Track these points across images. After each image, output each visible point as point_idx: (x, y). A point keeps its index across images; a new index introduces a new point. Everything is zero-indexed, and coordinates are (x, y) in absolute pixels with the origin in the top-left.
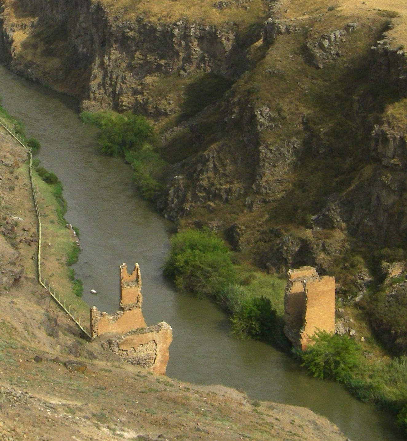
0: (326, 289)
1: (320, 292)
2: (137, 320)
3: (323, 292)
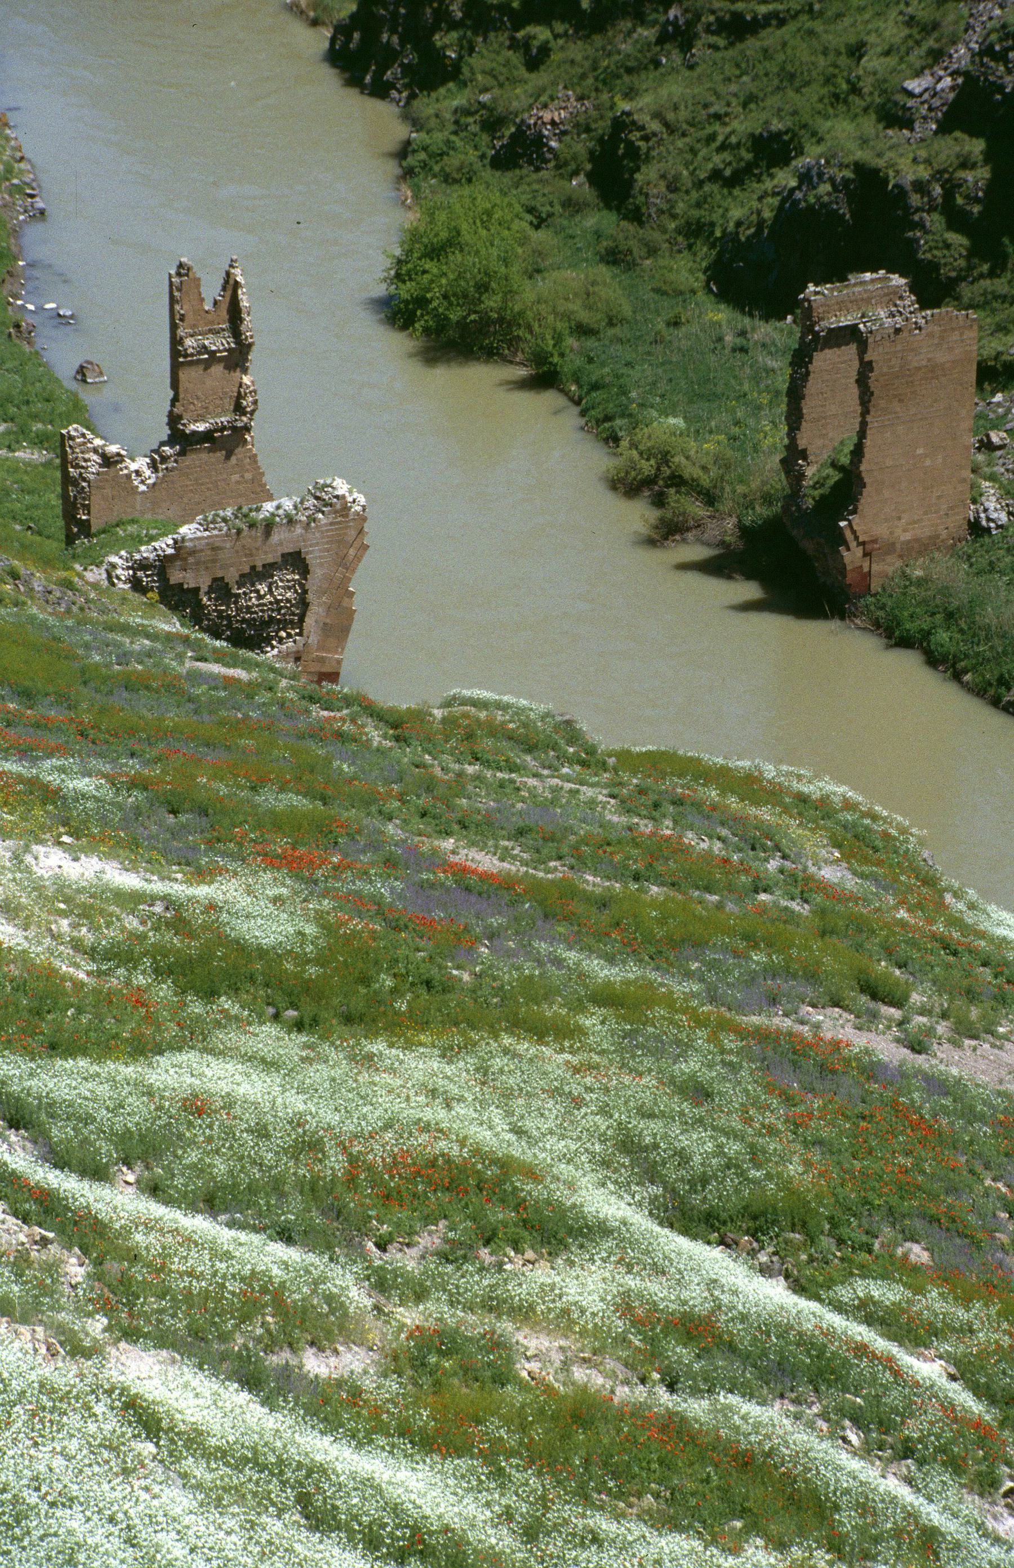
0: (942, 357)
1: (919, 369)
2: (236, 477)
3: (934, 370)
